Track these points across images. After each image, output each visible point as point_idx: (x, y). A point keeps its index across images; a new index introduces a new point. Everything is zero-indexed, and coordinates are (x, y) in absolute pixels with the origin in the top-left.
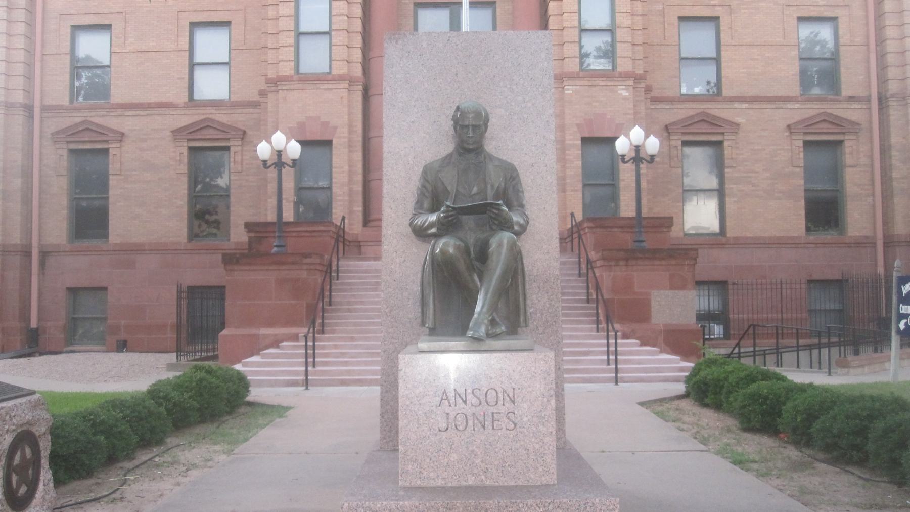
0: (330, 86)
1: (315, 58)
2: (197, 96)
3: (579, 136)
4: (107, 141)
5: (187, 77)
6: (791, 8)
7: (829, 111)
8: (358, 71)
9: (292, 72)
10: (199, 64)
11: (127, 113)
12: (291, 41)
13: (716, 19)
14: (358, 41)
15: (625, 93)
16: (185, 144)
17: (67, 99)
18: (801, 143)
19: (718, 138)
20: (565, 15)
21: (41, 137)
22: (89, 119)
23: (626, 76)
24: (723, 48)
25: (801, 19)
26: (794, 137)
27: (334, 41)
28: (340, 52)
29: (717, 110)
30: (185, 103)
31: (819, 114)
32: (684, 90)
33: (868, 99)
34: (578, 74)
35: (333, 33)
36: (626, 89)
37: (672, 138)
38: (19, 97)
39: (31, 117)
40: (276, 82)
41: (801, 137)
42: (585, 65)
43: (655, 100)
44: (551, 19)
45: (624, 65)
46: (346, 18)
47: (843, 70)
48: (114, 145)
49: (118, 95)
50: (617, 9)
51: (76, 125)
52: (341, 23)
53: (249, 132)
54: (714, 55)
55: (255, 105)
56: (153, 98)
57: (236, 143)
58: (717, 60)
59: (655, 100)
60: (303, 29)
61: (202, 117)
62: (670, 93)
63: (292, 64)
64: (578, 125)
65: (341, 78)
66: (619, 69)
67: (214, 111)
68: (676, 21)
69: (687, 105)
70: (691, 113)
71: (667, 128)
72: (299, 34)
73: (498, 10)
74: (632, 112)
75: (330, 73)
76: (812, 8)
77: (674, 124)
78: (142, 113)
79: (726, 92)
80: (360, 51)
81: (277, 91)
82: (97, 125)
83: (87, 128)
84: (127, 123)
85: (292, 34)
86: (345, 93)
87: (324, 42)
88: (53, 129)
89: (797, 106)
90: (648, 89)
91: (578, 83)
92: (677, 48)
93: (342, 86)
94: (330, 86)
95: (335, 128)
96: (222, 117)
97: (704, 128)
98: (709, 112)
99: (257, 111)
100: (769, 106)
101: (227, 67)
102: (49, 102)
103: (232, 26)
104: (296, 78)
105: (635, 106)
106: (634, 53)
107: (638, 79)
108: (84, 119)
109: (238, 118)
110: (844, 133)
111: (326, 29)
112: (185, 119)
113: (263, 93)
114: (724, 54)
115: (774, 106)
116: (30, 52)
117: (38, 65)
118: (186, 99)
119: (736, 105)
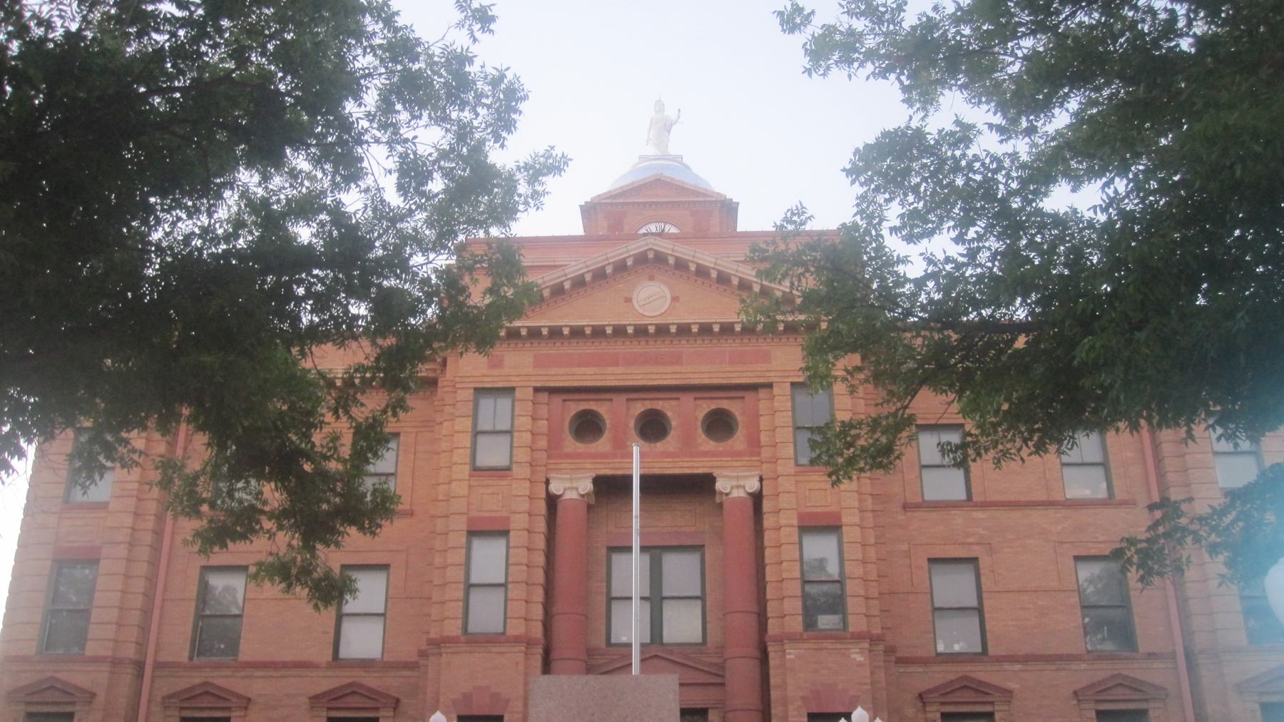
0: (503, 650)
1: (487, 614)
2: (343, 654)
3: (805, 712)
4: (229, 709)
5: (332, 631)
6: (1065, 546)
7: (1125, 673)
8: (538, 631)
9: (460, 632)
10: (348, 615)
11: (257, 674)
12: (461, 594)
13: (974, 560)
14: (539, 594)
15: (859, 658)
16: (324, 714)
17: (186, 654)
18: (1093, 714)
19: (987, 709)
20: (784, 564)
21: (149, 702)
22: (210, 680)
23: (859, 637)
24: (984, 595)
25: (1078, 558)
26: (1083, 706)
27: (510, 595)
28: (518, 609)
29: (982, 673)
30: (328, 663)
31: (1113, 677)
32: (941, 648)
33: (1173, 656)
34: (801, 635)
35: (510, 586)
36: (861, 653)
37: (928, 709)
38: (130, 652)
39: (140, 676)
40: (438, 644)
41: (1092, 706)
42: (965, 260)
43: (901, 661)
44: (768, 569)
45: (856, 623)
46: (525, 568)
47: (1137, 619)
48: (237, 714)
49: (249, 649)
50: (846, 556)
51: (193, 688)
52: (519, 573)
53: (404, 700)
54: (974, 603)
55: (412, 666)
56: (289, 656)
57: (386, 714)
58: (980, 610)
59: (901, 661)
60: (474, 580)
61: (347, 681)
62: (921, 653)
63: (460, 622)
64: (803, 698)
65: (517, 640)
66: (851, 629)
67: (362, 673)
68: (926, 565)
69: (944, 667)
70: (952, 677)
71: (921, 696)
72: (469, 587)
73: (707, 556)
74: (868, 681)
75: (504, 633)
76: (1091, 545)
77: (930, 691)
78: (274, 674)
79: (992, 651)
80: (540, 606)
81: (440, 654)
82: (219, 688)
83: (208, 691)
84: (256, 686)
85: (462, 586)
86: (521, 658)
87: (499, 595)
88: (165, 691)
89: (1083, 666)
90: (890, 650)
91: (801, 645)
92: (929, 596)
93: (517, 649)
94: (503, 650)
95: (508, 701)
96: (371, 680)
97: (968, 696)
98: (973, 675)
99: (416, 674)
100: (1048, 667)
101: (382, 619)
102: (165, 657)
103: (391, 570)
104: (463, 638)
105: (872, 673)
106: (867, 608)
107: (874, 640)
108: (203, 680)
109: (390, 683)
110: (1147, 700)
111: (502, 581)
112: (326, 682)
113: (423, 654)
114: (986, 603)
115: (1053, 667)
116: (149, 596)
117: (156, 612)
118: (330, 659)
119: (1007, 666)
